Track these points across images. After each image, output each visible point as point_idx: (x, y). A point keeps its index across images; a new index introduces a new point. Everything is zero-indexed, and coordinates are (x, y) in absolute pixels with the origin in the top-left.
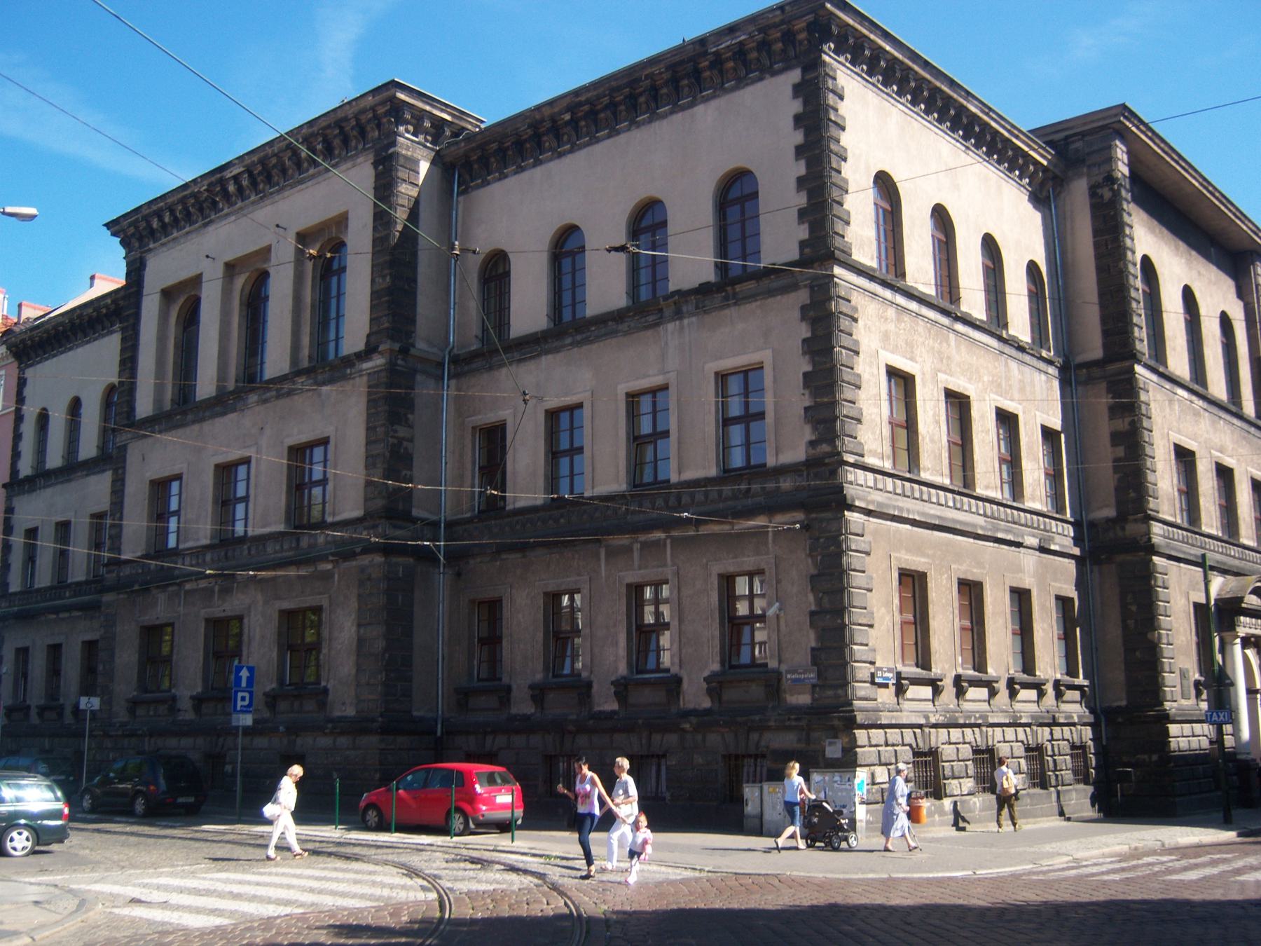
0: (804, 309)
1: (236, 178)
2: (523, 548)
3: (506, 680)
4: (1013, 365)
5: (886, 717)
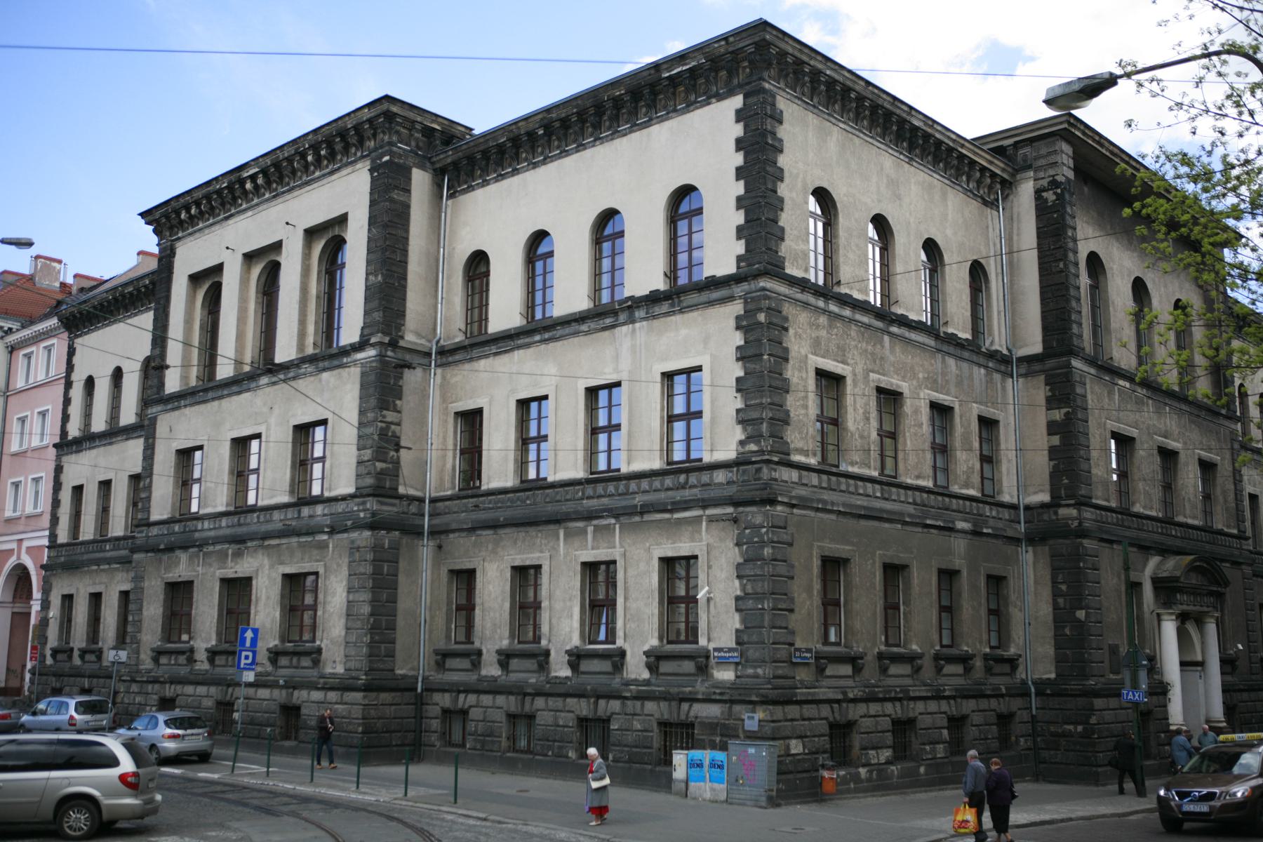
0: (738, 318)
1: (253, 178)
2: (494, 526)
3: (477, 644)
4: (951, 362)
5: (802, 694)
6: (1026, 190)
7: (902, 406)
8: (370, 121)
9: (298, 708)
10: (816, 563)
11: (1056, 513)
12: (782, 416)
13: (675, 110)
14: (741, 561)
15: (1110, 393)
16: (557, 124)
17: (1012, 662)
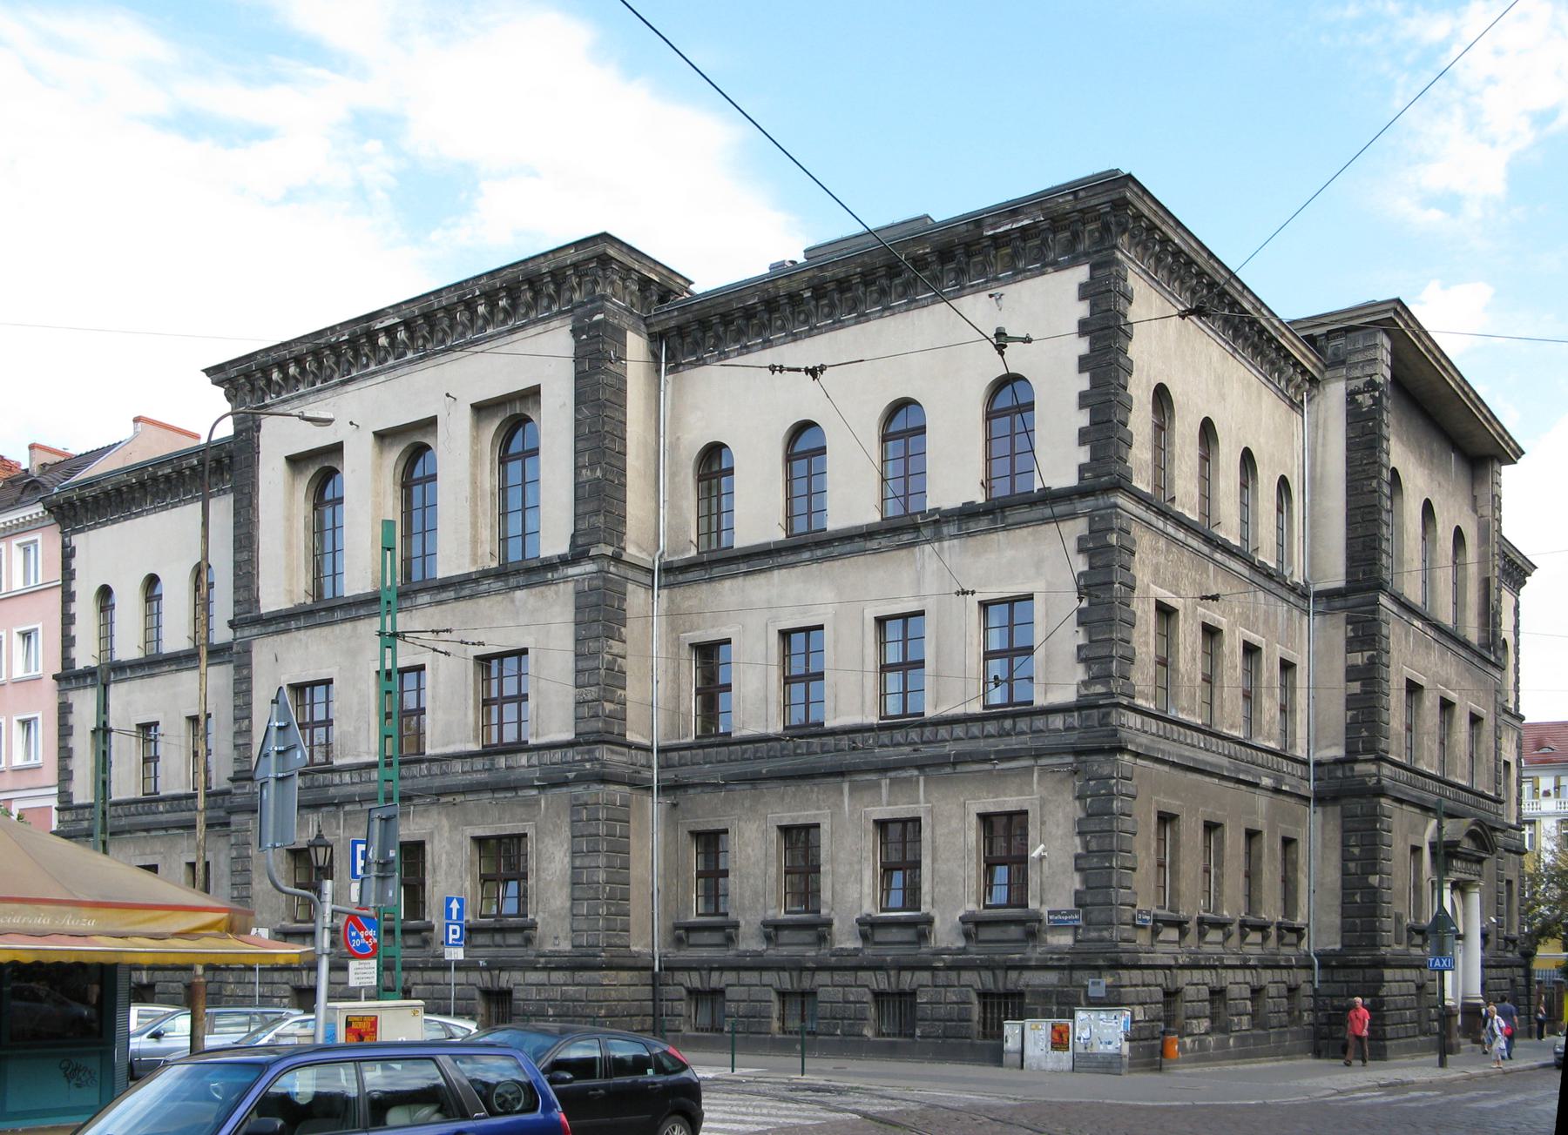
1: (390, 331)
2: (754, 780)
6: (1335, 394)
7: (1221, 645)
8: (575, 265)
9: (509, 993)
10: (1154, 818)
11: (1352, 770)
12: (1128, 654)
13: (996, 279)
14: (1082, 815)
15: (1407, 635)
16: (831, 286)
17: (1298, 931)
